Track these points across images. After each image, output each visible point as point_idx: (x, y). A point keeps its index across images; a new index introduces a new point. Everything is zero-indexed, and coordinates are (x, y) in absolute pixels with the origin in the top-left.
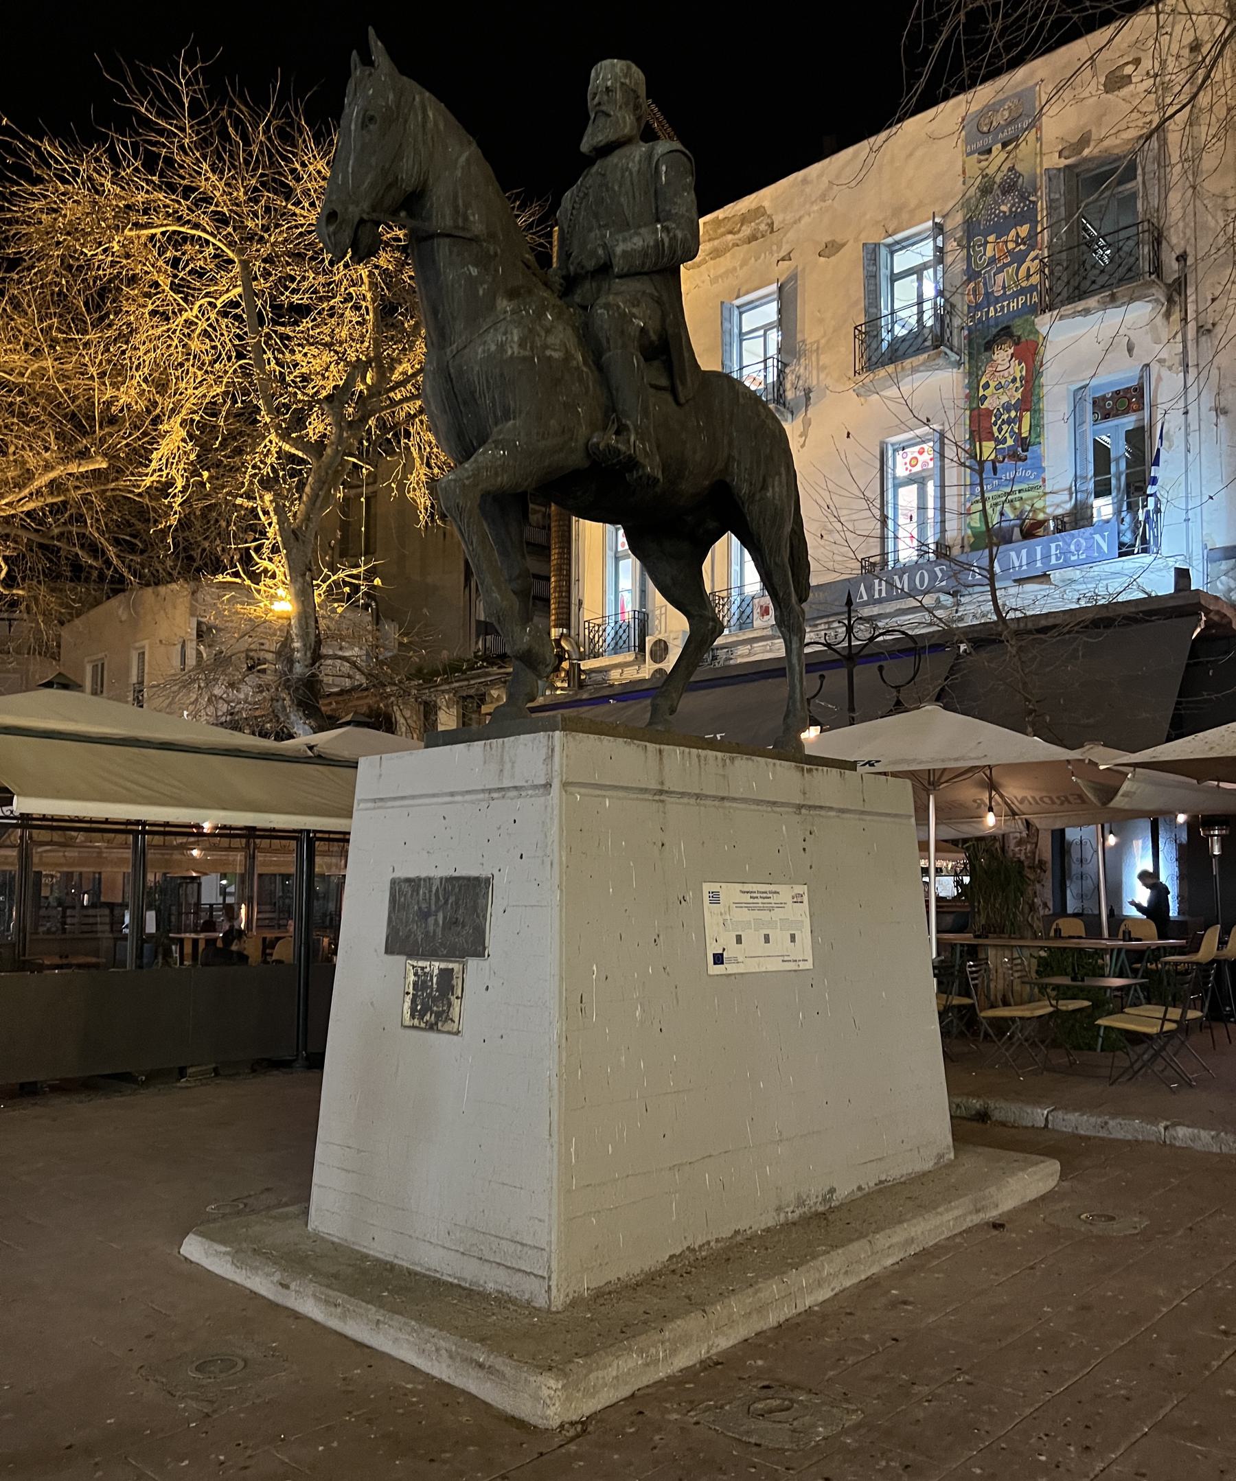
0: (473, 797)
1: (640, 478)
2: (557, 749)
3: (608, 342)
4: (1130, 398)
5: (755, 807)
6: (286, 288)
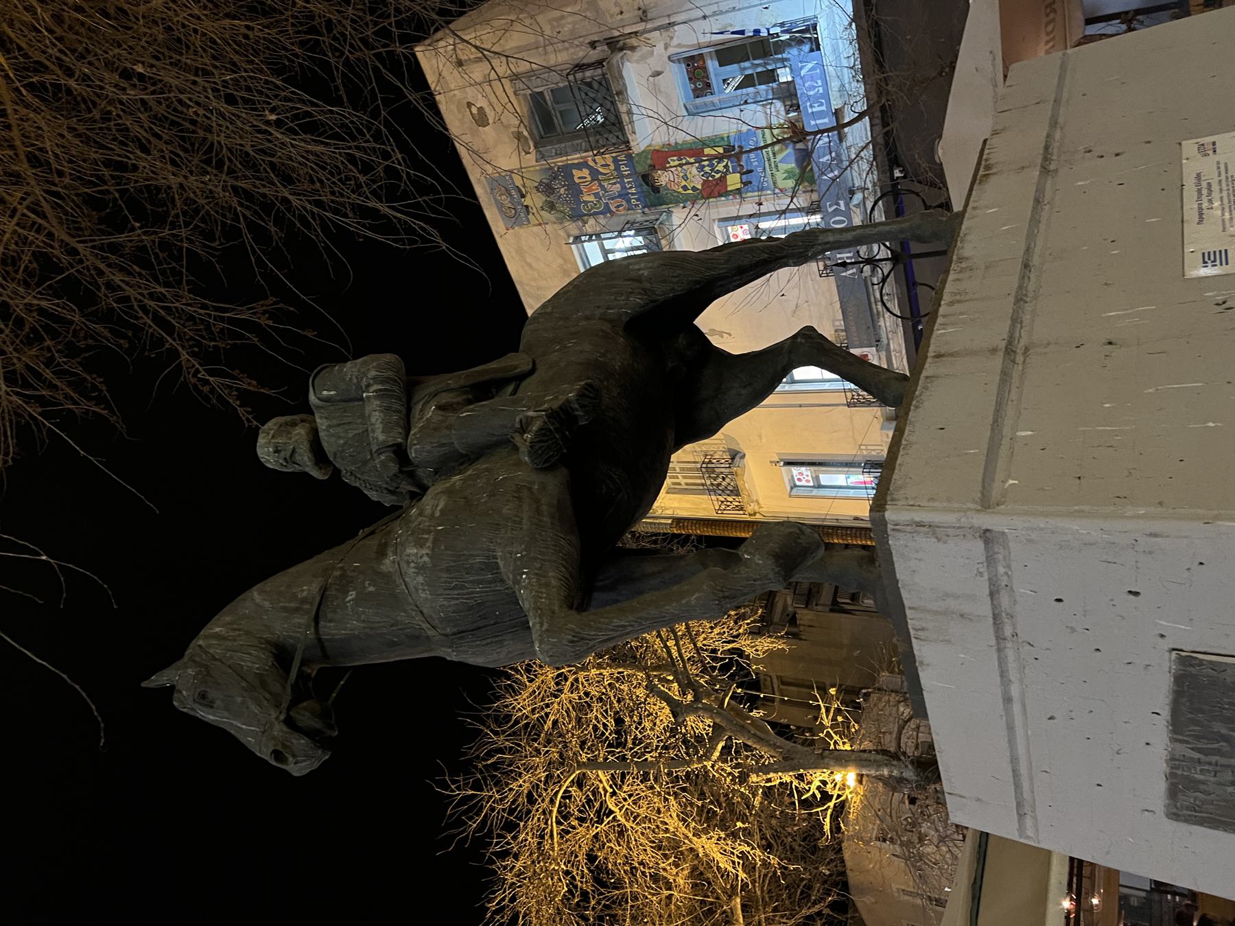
0: (1012, 666)
1: (582, 406)
2: (918, 516)
3: (444, 445)
4: (694, 67)
5: (1042, 227)
6: (603, 734)
